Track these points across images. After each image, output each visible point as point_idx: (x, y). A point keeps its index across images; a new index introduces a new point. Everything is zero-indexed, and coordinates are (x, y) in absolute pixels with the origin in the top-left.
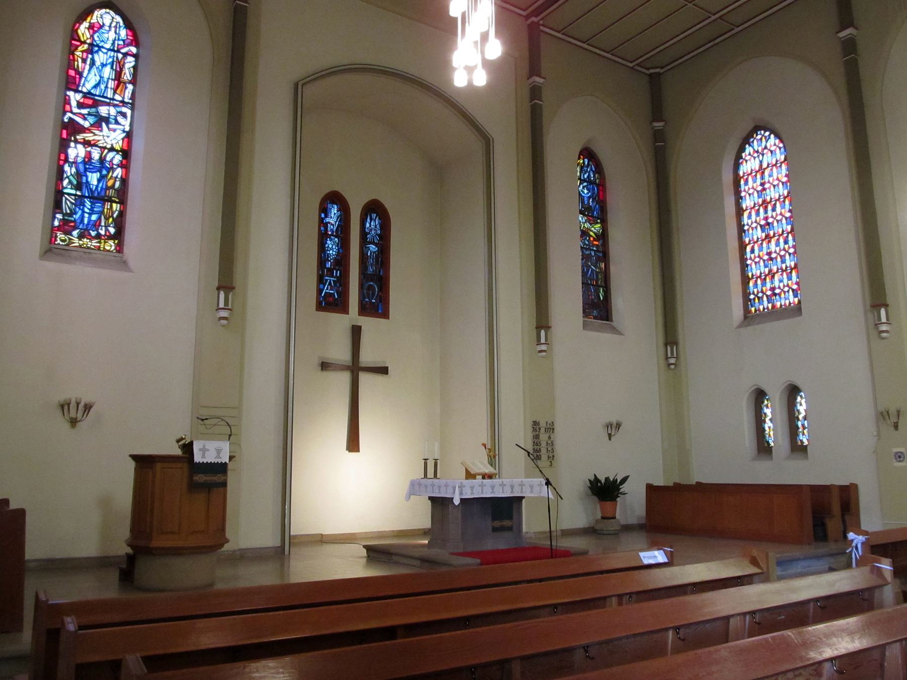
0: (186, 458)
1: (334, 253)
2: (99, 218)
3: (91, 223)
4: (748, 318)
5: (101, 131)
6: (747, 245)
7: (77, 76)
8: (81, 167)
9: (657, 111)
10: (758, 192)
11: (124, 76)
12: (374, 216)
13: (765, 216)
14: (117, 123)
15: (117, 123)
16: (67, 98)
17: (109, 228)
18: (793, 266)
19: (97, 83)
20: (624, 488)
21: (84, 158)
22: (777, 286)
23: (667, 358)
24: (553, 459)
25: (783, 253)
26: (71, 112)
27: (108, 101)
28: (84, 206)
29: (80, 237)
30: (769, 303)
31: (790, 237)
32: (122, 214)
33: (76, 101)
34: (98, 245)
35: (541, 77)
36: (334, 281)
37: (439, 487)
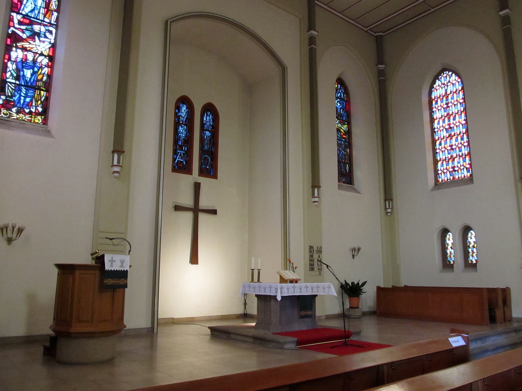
0: (98, 267)
1: (184, 135)
2: (32, 101)
3: (26, 103)
4: (438, 185)
5: (35, 41)
6: (436, 141)
7: (19, 3)
8: (20, 67)
9: (380, 60)
10: (444, 108)
11: (51, 6)
12: (209, 113)
13: (449, 123)
14: (46, 37)
15: (46, 37)
16: (11, 17)
17: (38, 108)
18: (467, 154)
19: (32, 9)
20: (365, 288)
21: (22, 59)
22: (456, 166)
23: (386, 209)
24: (321, 270)
25: (460, 145)
26: (14, 27)
27: (40, 22)
28: (21, 91)
29: (18, 112)
30: (451, 176)
31: (465, 136)
32: (47, 99)
33: (18, 20)
34: (30, 118)
35: (315, 31)
36: (183, 153)
37: (324, 288)
